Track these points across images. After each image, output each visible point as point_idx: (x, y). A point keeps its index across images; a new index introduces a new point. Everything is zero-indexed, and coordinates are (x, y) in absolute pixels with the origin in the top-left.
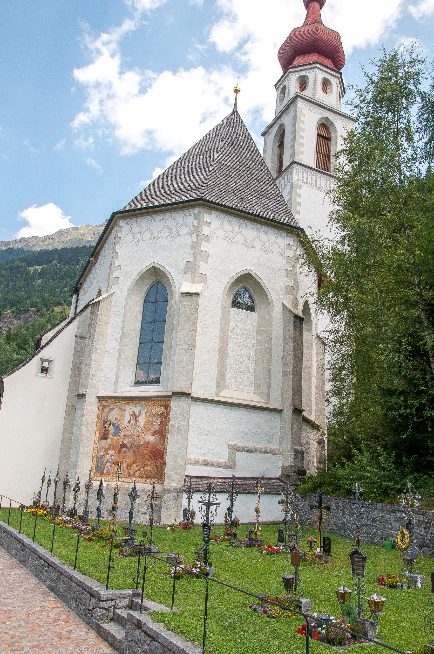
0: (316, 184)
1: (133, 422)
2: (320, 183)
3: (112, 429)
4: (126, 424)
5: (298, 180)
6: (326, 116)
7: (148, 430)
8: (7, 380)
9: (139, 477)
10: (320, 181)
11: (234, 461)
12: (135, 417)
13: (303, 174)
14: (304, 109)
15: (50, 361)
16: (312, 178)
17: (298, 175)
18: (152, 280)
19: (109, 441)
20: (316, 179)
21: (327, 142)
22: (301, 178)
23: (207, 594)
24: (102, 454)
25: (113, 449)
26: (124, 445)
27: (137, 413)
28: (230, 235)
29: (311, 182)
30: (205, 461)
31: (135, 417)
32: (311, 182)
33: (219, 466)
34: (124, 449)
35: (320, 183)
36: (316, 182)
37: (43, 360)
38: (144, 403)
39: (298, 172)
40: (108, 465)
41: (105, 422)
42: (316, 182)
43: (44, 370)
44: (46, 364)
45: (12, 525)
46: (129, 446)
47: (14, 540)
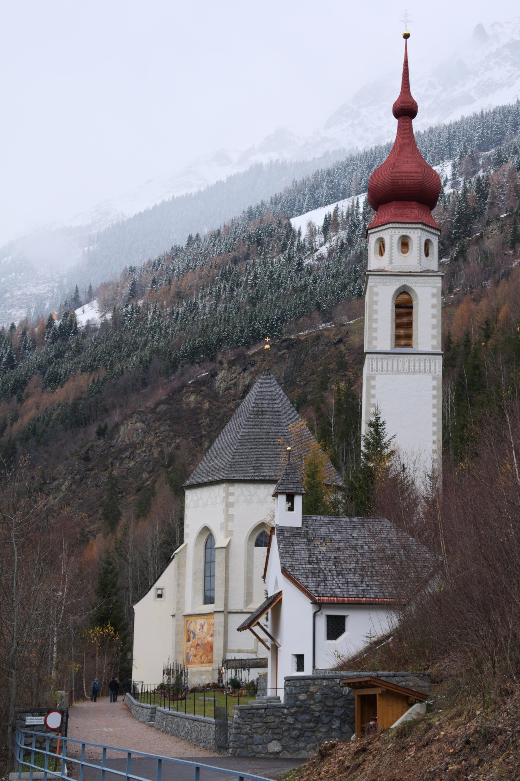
0: (393, 369)
1: (201, 630)
2: (398, 366)
3: (192, 635)
4: (198, 631)
5: (372, 371)
6: (404, 284)
7: (208, 634)
8: (136, 607)
9: (206, 663)
10: (398, 363)
11: (257, 649)
12: (202, 626)
13: (377, 362)
14: (376, 286)
15: (162, 589)
16: (387, 363)
17: (372, 365)
18: (207, 534)
19: (191, 642)
20: (393, 362)
21: (408, 311)
22: (375, 367)
23: (204, 711)
24: (188, 651)
25: (193, 647)
26: (198, 645)
27: (203, 624)
28: (248, 498)
29: (387, 368)
30: (239, 650)
31: (202, 626)
32: (387, 368)
33: (247, 652)
34: (198, 647)
35: (398, 366)
36: (393, 366)
37: (158, 589)
38: (206, 617)
39: (372, 362)
40: (192, 657)
41: (188, 631)
42: (393, 366)
43: (160, 596)
44: (159, 592)
45: (189, 713)
46: (200, 644)
47: (184, 720)
